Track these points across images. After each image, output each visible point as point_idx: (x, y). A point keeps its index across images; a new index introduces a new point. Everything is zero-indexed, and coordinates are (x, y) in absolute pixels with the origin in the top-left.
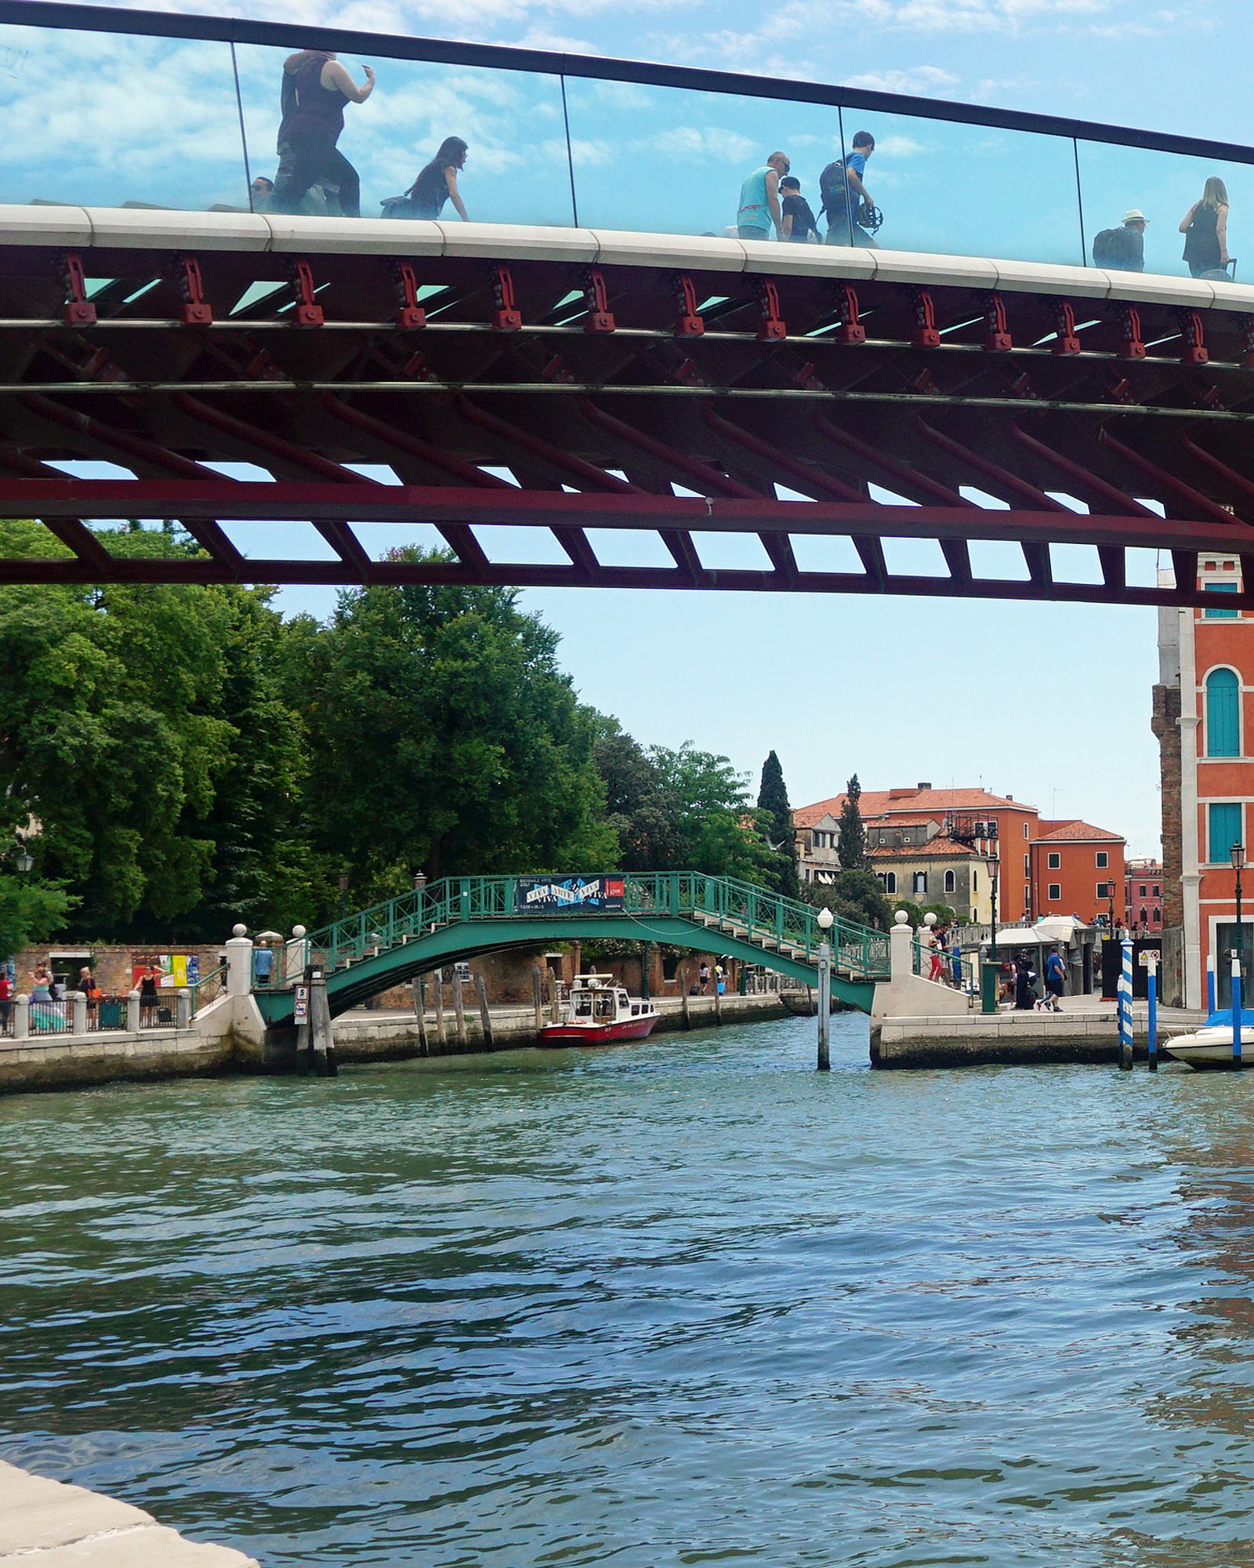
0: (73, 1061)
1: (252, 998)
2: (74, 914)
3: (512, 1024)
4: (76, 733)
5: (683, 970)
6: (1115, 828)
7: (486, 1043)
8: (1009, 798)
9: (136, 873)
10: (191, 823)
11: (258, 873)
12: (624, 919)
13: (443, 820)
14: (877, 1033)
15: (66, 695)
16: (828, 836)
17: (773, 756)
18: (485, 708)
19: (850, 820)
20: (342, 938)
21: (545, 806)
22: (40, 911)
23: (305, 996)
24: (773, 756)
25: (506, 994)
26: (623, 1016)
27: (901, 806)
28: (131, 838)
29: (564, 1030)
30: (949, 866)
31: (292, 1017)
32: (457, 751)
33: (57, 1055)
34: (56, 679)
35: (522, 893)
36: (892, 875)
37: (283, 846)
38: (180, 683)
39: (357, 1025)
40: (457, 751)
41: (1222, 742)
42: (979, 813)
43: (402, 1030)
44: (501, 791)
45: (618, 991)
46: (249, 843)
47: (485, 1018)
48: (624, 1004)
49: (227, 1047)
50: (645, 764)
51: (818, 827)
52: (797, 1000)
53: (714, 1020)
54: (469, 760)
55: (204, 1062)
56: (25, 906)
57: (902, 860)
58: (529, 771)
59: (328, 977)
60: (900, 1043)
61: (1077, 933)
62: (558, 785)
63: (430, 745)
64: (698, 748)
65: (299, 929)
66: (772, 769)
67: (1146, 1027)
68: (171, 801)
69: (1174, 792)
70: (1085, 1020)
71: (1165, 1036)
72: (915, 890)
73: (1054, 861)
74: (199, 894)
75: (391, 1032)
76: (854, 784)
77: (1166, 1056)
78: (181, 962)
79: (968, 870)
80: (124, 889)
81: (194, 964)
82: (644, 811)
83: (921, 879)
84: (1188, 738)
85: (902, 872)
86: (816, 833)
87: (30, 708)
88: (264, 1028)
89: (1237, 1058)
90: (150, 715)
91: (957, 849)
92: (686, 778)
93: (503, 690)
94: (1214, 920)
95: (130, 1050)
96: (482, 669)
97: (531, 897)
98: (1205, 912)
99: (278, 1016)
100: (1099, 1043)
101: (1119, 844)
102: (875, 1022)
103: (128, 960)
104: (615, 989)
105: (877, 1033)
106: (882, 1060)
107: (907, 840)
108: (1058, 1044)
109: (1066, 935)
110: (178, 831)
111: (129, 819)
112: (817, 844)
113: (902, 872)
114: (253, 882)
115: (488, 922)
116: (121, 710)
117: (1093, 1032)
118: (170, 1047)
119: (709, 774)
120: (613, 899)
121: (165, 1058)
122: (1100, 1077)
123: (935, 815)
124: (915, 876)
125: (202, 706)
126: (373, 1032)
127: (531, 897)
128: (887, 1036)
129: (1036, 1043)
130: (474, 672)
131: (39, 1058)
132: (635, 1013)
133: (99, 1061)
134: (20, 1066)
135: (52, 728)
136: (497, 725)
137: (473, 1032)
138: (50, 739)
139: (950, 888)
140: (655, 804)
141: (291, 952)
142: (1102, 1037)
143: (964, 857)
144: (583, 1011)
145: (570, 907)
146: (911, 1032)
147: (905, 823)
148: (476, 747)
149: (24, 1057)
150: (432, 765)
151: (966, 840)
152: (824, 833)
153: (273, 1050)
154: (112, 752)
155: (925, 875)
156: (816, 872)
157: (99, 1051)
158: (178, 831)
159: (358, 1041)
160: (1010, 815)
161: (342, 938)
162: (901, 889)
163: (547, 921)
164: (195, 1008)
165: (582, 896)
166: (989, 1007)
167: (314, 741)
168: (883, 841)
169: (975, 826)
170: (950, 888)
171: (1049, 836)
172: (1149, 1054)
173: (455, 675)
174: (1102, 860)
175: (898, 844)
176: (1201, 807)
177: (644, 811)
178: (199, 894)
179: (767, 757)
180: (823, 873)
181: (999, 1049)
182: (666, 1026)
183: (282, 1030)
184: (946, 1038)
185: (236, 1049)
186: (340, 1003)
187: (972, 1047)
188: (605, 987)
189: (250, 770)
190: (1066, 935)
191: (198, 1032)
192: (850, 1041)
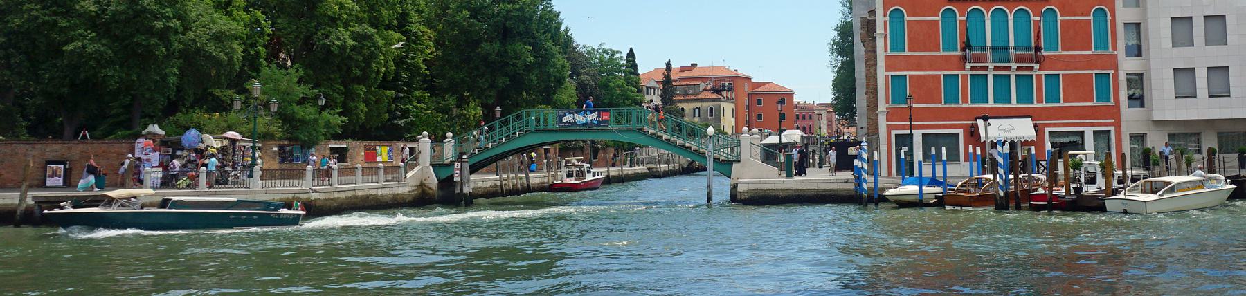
0: (356, 197)
2: (344, 127)
3: (538, 181)
4: (339, 39)
5: (601, 154)
6: (788, 86)
7: (529, 189)
9: (363, 107)
10: (385, 84)
11: (410, 107)
12: (609, 131)
13: (502, 81)
14: (735, 187)
15: (333, 21)
18: (522, 28)
19: (667, 81)
21: (549, 75)
22: (328, 125)
26: (589, 177)
27: (686, 74)
28: (361, 90)
29: (562, 184)
30: (711, 104)
31: (452, 176)
32: (509, 48)
33: (350, 194)
34: (330, 13)
35: (561, 117)
37: (417, 94)
38: (381, 15)
39: (482, 180)
40: (509, 48)
41: (897, 44)
42: (724, 78)
43: (492, 183)
44: (528, 68)
45: (586, 165)
46: (405, 92)
47: (527, 178)
50: (581, 54)
53: (622, 179)
54: (515, 52)
56: (322, 123)
57: (688, 101)
58: (543, 59)
59: (469, 157)
61: (802, 138)
62: (555, 65)
63: (497, 46)
64: (606, 47)
66: (631, 54)
67: (872, 186)
68: (378, 72)
69: (872, 69)
70: (822, 182)
71: (883, 190)
73: (760, 102)
74: (387, 116)
75: (488, 184)
76: (669, 64)
77: (884, 199)
78: (385, 149)
80: (357, 115)
81: (390, 151)
82: (583, 77)
84: (880, 43)
85: (688, 107)
87: (317, 27)
89: (921, 201)
90: (370, 30)
91: (715, 96)
92: (601, 61)
94: (894, 133)
95: (380, 192)
96: (522, 9)
97: (565, 119)
98: (889, 128)
99: (444, 175)
100: (844, 193)
101: (790, 94)
102: (735, 182)
103: (362, 148)
105: (735, 187)
106: (734, 198)
109: (798, 139)
110: (379, 87)
111: (361, 80)
113: (688, 107)
114: (407, 111)
116: (357, 28)
118: (396, 191)
119: (611, 60)
120: (604, 121)
121: (395, 196)
122: (850, 210)
123: (704, 79)
125: (388, 27)
126: (481, 184)
127: (565, 119)
128: (740, 188)
131: (342, 196)
133: (367, 197)
134: (334, 199)
135: (327, 37)
136: (527, 36)
137: (522, 185)
138: (327, 42)
144: (569, 175)
145: (584, 125)
146: (752, 187)
148: (518, 46)
149: (336, 195)
151: (719, 92)
153: (441, 193)
154: (354, 48)
157: (367, 193)
158: (379, 87)
163: (573, 131)
164: (406, 172)
166: (789, 175)
167: (439, 44)
169: (723, 85)
172: (877, 199)
173: (509, 11)
175: (686, 94)
176: (887, 77)
177: (583, 77)
178: (387, 116)
182: (608, 180)
183: (447, 183)
185: (424, 191)
186: (474, 169)
187: (782, 194)
189: (407, 57)
190: (798, 139)
191: (407, 185)
192: (722, 189)
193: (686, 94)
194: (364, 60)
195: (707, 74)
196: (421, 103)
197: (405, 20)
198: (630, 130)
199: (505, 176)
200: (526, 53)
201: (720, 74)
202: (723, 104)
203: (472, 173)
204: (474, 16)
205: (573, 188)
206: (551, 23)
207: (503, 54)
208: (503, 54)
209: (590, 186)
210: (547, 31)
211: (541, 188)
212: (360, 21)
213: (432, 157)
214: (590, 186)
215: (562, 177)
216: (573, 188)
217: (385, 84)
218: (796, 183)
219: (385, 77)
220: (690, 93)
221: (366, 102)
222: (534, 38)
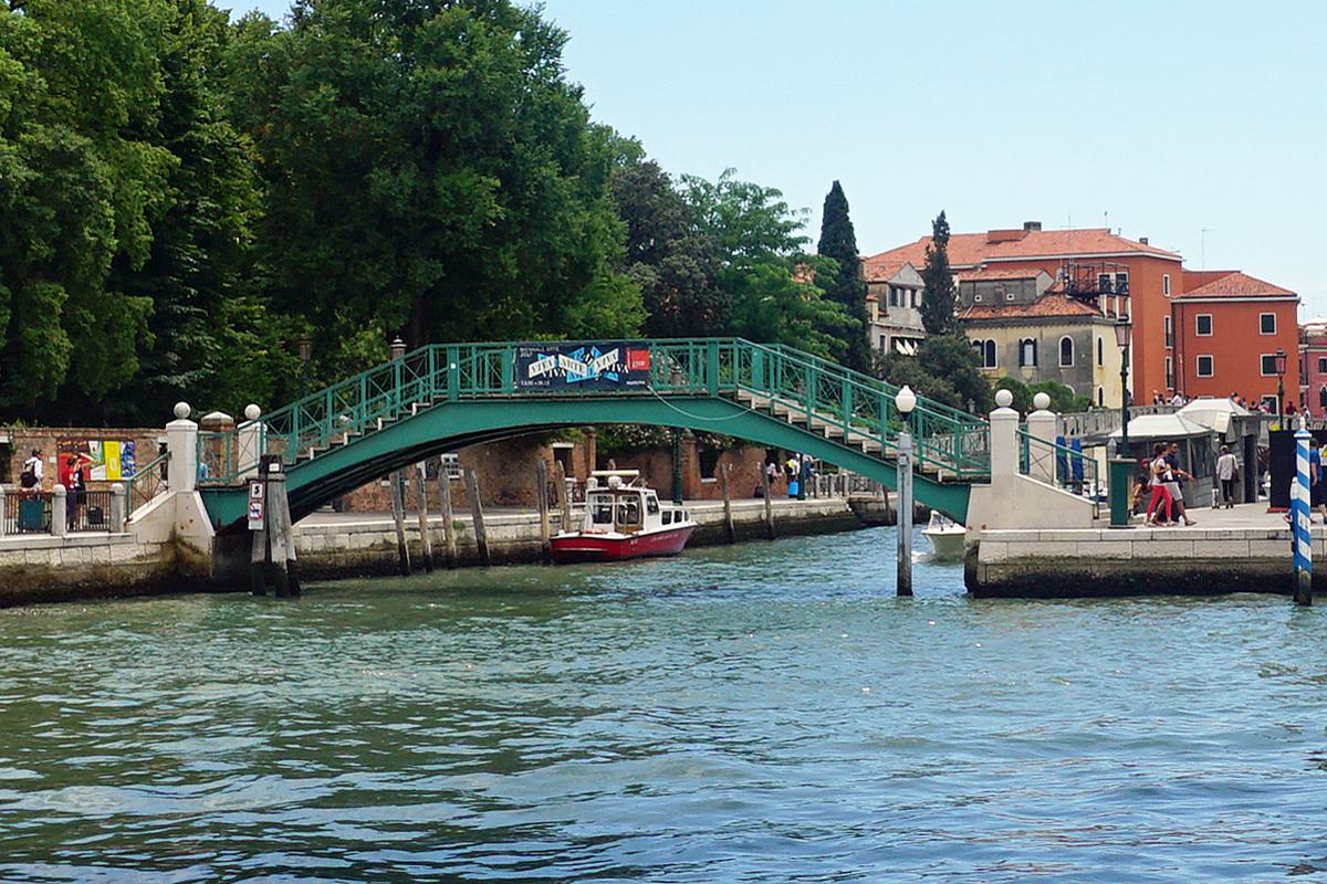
1: (197, 495)
3: (511, 533)
5: (725, 466)
6: (1283, 281)
7: (481, 555)
8: (1144, 241)
9: (60, 338)
10: (124, 276)
11: (205, 339)
13: (426, 271)
16: (908, 292)
17: (837, 188)
19: (937, 271)
21: (551, 254)
23: (260, 495)
24: (837, 188)
25: (505, 494)
26: (652, 525)
28: (54, 294)
29: (580, 541)
31: (244, 521)
35: (523, 366)
36: (991, 344)
38: (110, 101)
43: (378, 539)
44: (496, 235)
45: (646, 493)
46: (194, 302)
48: (653, 510)
49: (169, 556)
50: (676, 200)
51: (895, 281)
52: (870, 506)
53: (766, 531)
54: (457, 194)
55: (142, 576)
58: (530, 211)
60: (1004, 564)
61: (1235, 420)
63: (408, 177)
64: (741, 178)
66: (836, 205)
68: (100, 248)
72: (1022, 363)
73: (1204, 325)
74: (134, 364)
75: (365, 541)
76: (941, 224)
78: (114, 449)
79: (1090, 337)
80: (46, 358)
81: (129, 452)
82: (674, 260)
83: (1029, 349)
85: (1004, 339)
86: (894, 288)
91: (1076, 309)
92: (726, 217)
93: (497, 105)
95: (56, 559)
97: (534, 370)
99: (228, 519)
101: (1290, 303)
104: (641, 490)
107: (1010, 297)
108: (1211, 568)
110: (110, 285)
111: (58, 269)
112: (894, 303)
113: (1004, 339)
115: (482, 402)
116: (41, 135)
117: (1259, 554)
118: (101, 556)
120: (635, 374)
123: (1046, 264)
124: (1022, 345)
125: (135, 130)
126: (343, 541)
127: (534, 370)
129: (1182, 568)
130: (463, 83)
132: (666, 521)
133: (20, 571)
136: (490, 150)
139: (1067, 361)
140: (688, 251)
141: (243, 438)
142: (1270, 560)
143: (1086, 319)
144: (602, 517)
145: (582, 384)
146: (1018, 551)
147: (1007, 275)
148: (465, 178)
150: (412, 202)
151: (1087, 297)
152: (903, 288)
154: (33, 188)
155: (1034, 343)
156: (894, 340)
157: (19, 559)
158: (110, 285)
159: (324, 552)
160: (1145, 265)
162: (1004, 362)
163: (554, 401)
165: (597, 370)
168: (979, 299)
169: (1099, 278)
170: (1067, 361)
173: (440, 86)
174: (1268, 324)
175: (999, 302)
177: (674, 260)
178: (134, 364)
179: (829, 189)
180: (902, 340)
181: (1134, 574)
182: (708, 538)
183: (233, 536)
184: (1063, 558)
185: (179, 558)
186: (302, 504)
187: (1098, 571)
188: (629, 488)
189: (192, 209)
190: (1221, 424)
191: (131, 542)
193: (999, 302)
194: (61, 218)
195: (1060, 252)
196: (253, 329)
197: (186, 113)
198: (700, 398)
199: (413, 520)
200: (483, 192)
201: (1095, 249)
202: (1098, 332)
203: (295, 518)
204: (348, 97)
205: (610, 553)
206: (558, 116)
207: (424, 199)
208: (424, 199)
209: (650, 550)
210: (548, 138)
211: (523, 554)
212: (46, 116)
213: (200, 473)
214: (650, 550)
215: (583, 522)
216: (610, 553)
217: (124, 276)
218: (1143, 539)
219: (122, 259)
220: (1001, 305)
221: (72, 327)
222: (507, 154)
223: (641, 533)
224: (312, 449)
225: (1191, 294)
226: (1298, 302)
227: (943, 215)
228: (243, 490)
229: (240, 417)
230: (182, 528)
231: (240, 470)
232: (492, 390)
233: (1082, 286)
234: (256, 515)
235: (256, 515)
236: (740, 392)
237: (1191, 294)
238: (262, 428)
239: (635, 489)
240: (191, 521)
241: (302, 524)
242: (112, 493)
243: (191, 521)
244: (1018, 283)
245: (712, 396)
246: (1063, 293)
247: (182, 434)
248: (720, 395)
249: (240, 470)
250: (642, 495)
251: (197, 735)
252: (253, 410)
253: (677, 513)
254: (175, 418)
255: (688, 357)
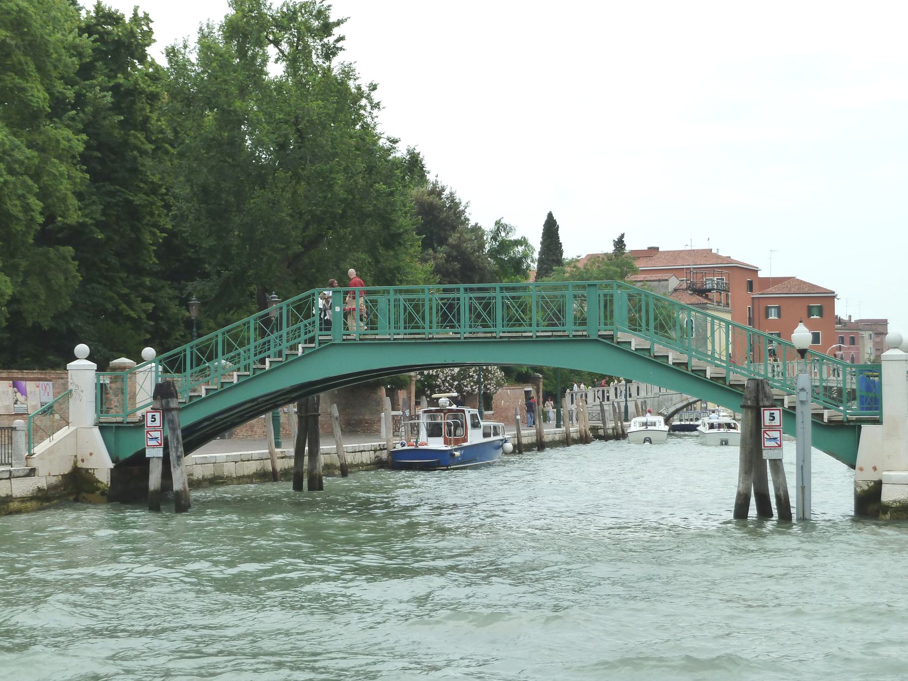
1: (96, 430)
17: (550, 215)
20: (229, 347)
24: (550, 215)
26: (475, 437)
48: (475, 425)
65: (149, 352)
66: (551, 228)
88: (112, 465)
99: (127, 452)
101: (829, 298)
104: (466, 409)
106: (870, 505)
115: (362, 343)
132: (486, 435)
141: (140, 377)
151: (702, 292)
161: (229, 347)
171: (768, 290)
179: (545, 218)
186: (195, 437)
188: (454, 407)
223: (465, 444)
224: (203, 388)
225: (765, 291)
226: (834, 297)
227: (623, 236)
228: (139, 426)
229: (139, 359)
230: (83, 461)
231: (138, 406)
232: (505, 329)
233: (699, 285)
234: (154, 443)
235: (154, 443)
236: (619, 334)
237: (765, 291)
238: (157, 367)
239: (460, 408)
240: (91, 454)
241: (195, 455)
242: (13, 429)
243: (91, 454)
244: (656, 283)
245: (591, 338)
246: (686, 289)
247: (82, 369)
248: (599, 336)
249: (138, 406)
250: (466, 413)
251: (130, 636)
252: (149, 352)
253: (495, 428)
254: (76, 358)
255: (405, 323)
